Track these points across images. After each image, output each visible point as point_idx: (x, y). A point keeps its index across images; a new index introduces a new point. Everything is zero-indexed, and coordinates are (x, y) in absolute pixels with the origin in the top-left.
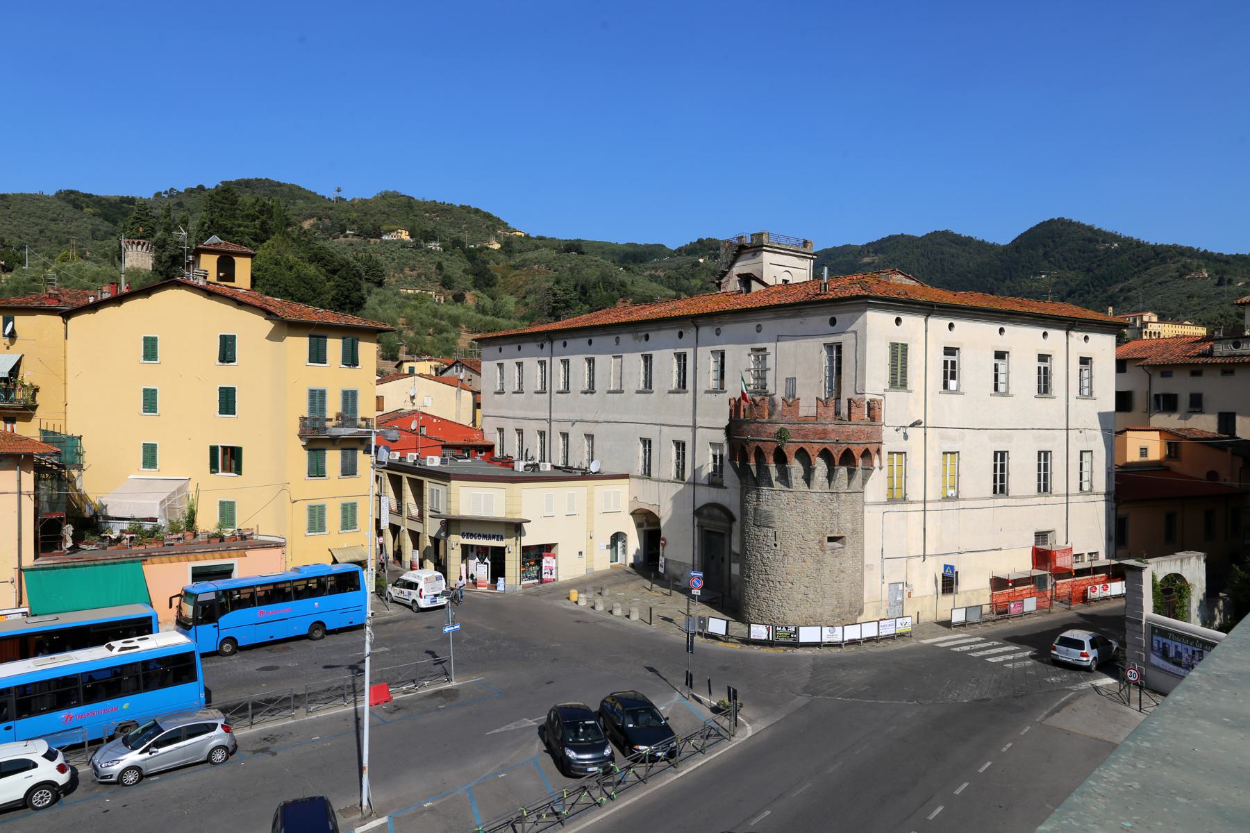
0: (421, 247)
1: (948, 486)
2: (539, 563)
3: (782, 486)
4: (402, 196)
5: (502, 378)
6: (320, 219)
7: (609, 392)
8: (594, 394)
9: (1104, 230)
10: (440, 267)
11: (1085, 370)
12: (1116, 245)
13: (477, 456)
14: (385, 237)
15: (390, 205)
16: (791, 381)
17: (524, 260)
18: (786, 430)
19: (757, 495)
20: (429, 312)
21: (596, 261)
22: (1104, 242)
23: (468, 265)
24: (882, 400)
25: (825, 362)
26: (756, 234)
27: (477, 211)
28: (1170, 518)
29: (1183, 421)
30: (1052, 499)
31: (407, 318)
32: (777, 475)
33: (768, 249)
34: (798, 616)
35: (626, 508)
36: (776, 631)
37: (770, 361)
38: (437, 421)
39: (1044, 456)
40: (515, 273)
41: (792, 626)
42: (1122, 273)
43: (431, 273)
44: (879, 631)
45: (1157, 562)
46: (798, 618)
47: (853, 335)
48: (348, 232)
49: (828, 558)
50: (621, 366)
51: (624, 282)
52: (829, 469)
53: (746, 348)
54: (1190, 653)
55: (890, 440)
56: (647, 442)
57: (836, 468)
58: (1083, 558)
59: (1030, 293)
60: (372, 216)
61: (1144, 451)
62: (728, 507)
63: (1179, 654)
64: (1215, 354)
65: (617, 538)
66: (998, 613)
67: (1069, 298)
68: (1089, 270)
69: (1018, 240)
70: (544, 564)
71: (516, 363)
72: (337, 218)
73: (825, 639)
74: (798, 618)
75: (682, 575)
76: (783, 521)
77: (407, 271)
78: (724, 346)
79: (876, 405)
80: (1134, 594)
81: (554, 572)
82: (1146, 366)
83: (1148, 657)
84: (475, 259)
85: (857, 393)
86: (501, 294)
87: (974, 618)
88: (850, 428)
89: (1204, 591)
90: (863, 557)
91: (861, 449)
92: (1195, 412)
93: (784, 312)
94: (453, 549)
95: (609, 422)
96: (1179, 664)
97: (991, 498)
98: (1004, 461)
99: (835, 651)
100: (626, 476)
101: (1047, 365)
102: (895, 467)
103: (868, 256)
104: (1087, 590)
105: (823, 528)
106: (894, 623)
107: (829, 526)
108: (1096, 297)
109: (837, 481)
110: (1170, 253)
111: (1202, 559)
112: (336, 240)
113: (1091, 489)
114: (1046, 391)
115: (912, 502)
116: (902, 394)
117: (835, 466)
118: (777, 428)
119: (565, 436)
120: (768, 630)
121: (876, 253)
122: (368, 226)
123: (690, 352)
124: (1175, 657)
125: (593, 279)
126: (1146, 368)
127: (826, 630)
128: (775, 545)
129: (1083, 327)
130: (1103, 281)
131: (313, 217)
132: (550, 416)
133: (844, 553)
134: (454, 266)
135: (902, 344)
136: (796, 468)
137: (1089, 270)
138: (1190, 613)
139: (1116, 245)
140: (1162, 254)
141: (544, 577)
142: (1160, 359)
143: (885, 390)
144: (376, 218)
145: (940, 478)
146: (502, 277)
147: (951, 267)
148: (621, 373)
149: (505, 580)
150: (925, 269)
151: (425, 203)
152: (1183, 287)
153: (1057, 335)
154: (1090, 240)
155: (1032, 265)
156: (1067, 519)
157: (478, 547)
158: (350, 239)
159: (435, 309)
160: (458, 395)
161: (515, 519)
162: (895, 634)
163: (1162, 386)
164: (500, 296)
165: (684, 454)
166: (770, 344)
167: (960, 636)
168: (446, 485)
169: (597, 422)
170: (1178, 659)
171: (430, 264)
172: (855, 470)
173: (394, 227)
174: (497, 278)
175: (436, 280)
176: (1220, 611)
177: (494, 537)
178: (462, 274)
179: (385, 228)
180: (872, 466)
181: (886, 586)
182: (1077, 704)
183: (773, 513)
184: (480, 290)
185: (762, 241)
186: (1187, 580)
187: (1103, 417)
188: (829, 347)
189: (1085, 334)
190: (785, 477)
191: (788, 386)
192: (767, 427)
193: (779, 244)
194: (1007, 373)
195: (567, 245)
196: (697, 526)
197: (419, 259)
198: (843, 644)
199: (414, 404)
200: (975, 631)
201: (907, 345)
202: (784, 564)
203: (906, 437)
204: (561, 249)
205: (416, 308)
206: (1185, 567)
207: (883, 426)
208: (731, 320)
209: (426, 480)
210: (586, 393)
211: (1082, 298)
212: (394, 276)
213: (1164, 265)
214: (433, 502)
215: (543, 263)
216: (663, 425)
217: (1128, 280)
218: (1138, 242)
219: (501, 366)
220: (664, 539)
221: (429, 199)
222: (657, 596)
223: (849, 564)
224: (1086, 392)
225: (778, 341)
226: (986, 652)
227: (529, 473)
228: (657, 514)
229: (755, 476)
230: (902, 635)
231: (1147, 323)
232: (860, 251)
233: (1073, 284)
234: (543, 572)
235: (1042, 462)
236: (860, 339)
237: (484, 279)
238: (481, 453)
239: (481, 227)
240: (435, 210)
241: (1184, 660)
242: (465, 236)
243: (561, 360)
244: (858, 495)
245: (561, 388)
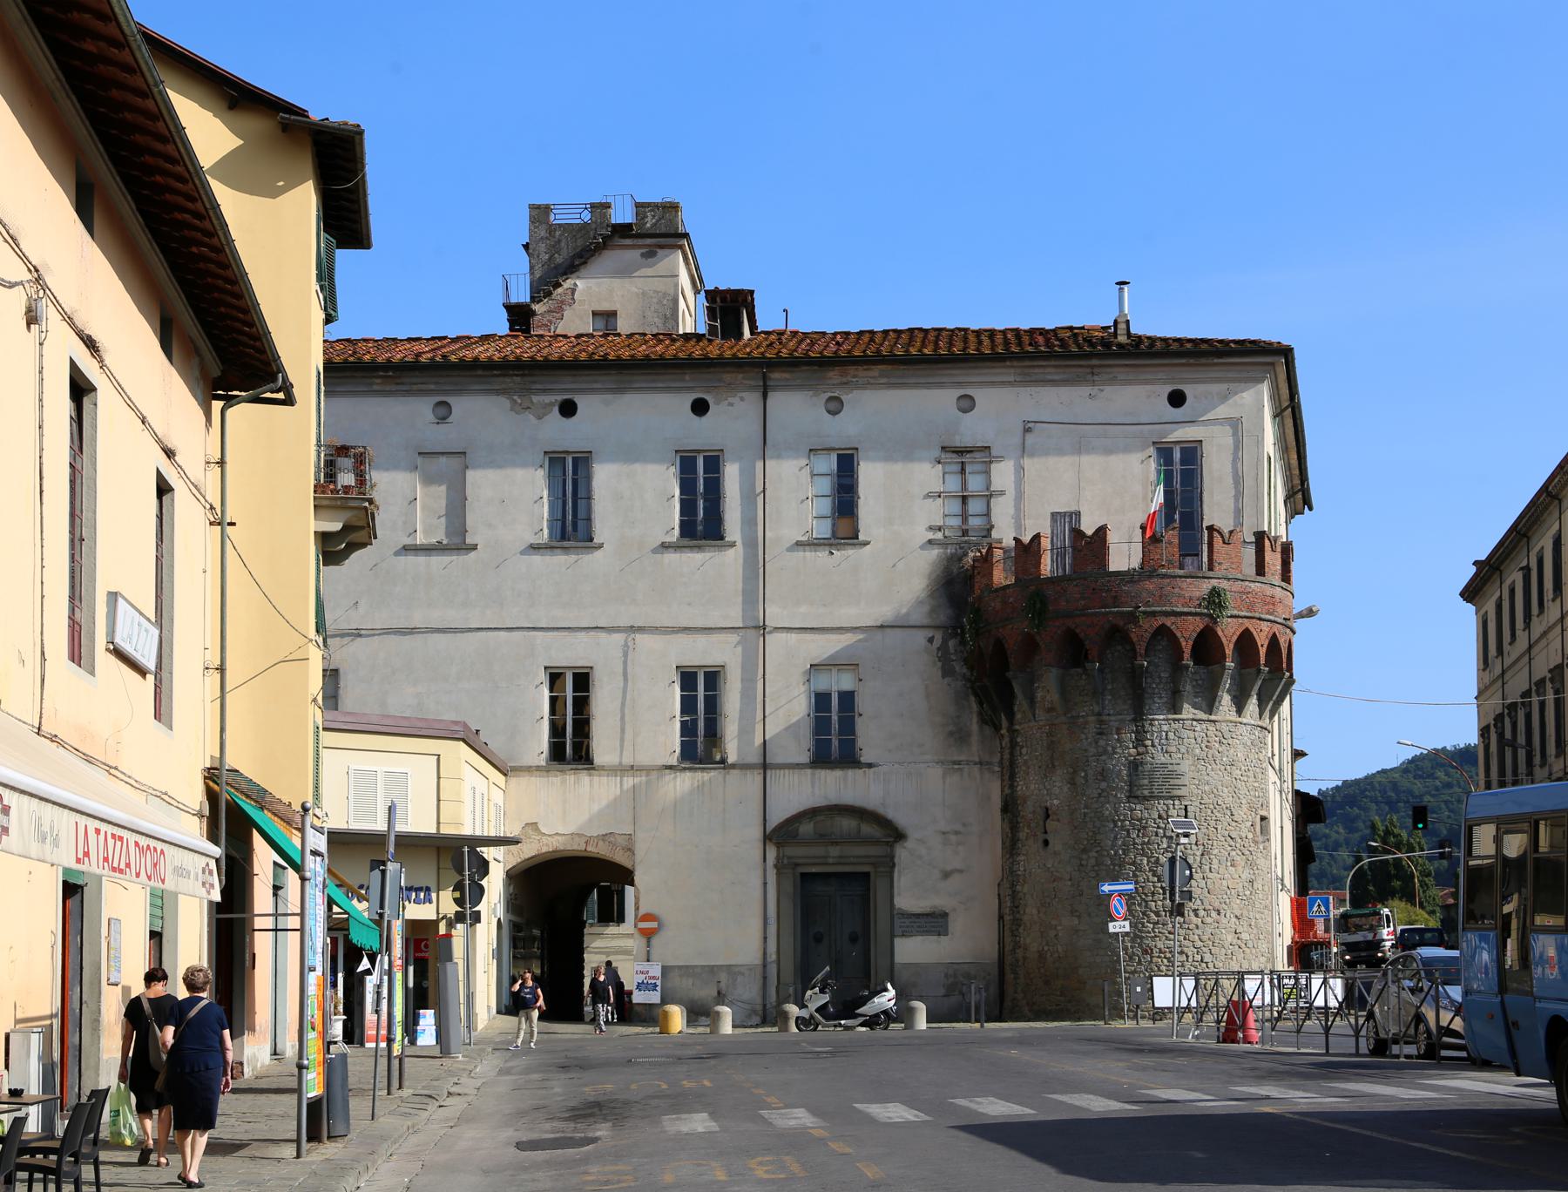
19: (1137, 732)
26: (655, 206)
62: (881, 811)
93: (1053, 370)
118: (1205, 587)
192: (1184, 585)
208: (884, 380)
216: (641, 629)
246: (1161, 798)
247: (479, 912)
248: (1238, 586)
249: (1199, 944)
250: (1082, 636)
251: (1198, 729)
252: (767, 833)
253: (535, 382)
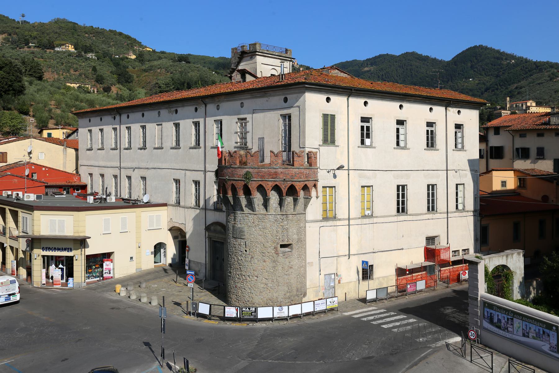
0: (82, 56)
1: (366, 208)
2: (102, 266)
3: (250, 211)
4: (69, 22)
5: (91, 140)
6: (10, 35)
7: (155, 148)
8: (146, 150)
9: (506, 52)
10: (94, 69)
11: (459, 132)
12: (513, 61)
13: (75, 192)
14: (57, 49)
15: (60, 28)
16: (262, 139)
17: (152, 66)
18: (250, 172)
20: (72, 97)
21: (198, 68)
22: (506, 59)
23: (114, 69)
24: (317, 152)
25: (282, 127)
26: (252, 44)
27: (121, 34)
28: (516, 226)
29: (533, 164)
30: (437, 216)
31: (56, 101)
32: (246, 203)
33: (260, 54)
34: (262, 299)
35: (165, 226)
36: (242, 311)
37: (249, 127)
38: (45, 169)
39: (431, 188)
40: (145, 75)
41: (253, 307)
42: (517, 77)
43: (88, 73)
44: (314, 308)
45: (490, 258)
46: (261, 301)
47: (298, 109)
48: (30, 44)
49: (281, 259)
50: (162, 131)
51: (214, 81)
52: (280, 198)
53: (235, 118)
54: (506, 320)
55: (324, 179)
56: (177, 181)
57: (284, 198)
58: (459, 253)
59: (463, 89)
60: (48, 34)
61: (504, 183)
63: (499, 320)
64: (551, 123)
65: (159, 248)
66: (400, 292)
67: (486, 93)
68: (497, 76)
69: (456, 58)
70: (105, 266)
71: (100, 129)
72: (22, 35)
73: (276, 315)
74: (261, 301)
75: (199, 271)
76: (251, 234)
77: (72, 71)
78: (221, 117)
79: (312, 155)
80: (474, 278)
81: (112, 272)
82: (510, 130)
83: (481, 322)
84: (119, 65)
85: (300, 148)
86: (136, 88)
87: (382, 295)
88: (293, 171)
89: (523, 275)
90: (305, 257)
91: (271, 184)
92: (540, 159)
93: (256, 94)
94: (36, 259)
95: (155, 168)
96: (499, 327)
97: (395, 216)
98: (404, 191)
99: (282, 323)
100: (165, 205)
101: (433, 129)
102: (328, 196)
103: (367, 67)
104: (460, 274)
105: (277, 239)
106: (325, 302)
107: (281, 237)
108: (501, 92)
109: (286, 207)
110: (544, 66)
111: (521, 255)
112: (21, 50)
113: (464, 209)
114: (432, 146)
115: (340, 220)
116: (331, 148)
117: (283, 196)
118: (244, 171)
119: (129, 178)
120: (237, 310)
121: (372, 64)
122: (45, 41)
123: (201, 121)
124: (497, 323)
125: (195, 79)
126: (511, 132)
127: (276, 309)
128: (246, 251)
129: (456, 104)
130: (506, 83)
131: (4, 33)
132: (120, 165)
133: (292, 255)
134: (104, 69)
135: (331, 115)
136: (258, 198)
137: (497, 76)
138: (513, 291)
139: (513, 61)
140: (539, 67)
141: (104, 275)
142: (519, 127)
143: (319, 146)
144: (51, 36)
145: (359, 204)
146: (137, 77)
147: (416, 74)
148: (162, 136)
149: (73, 279)
150: (401, 75)
151: (85, 27)
152: (552, 86)
153: (439, 110)
154: (498, 58)
155: (464, 73)
156: (448, 228)
157: (56, 257)
158: (32, 49)
159: (77, 95)
160: (64, 151)
161: (80, 237)
162: (326, 309)
163: (520, 143)
164: (136, 89)
165: (199, 189)
166: (249, 115)
167: (371, 309)
168: (31, 214)
169: (148, 168)
170: (499, 324)
171: (88, 67)
172: (297, 199)
173: (64, 42)
174: (133, 77)
175: (92, 78)
176: (534, 289)
177: (65, 249)
178: (110, 74)
179: (57, 42)
180: (310, 196)
181: (322, 276)
182: (431, 358)
183: (244, 229)
184: (122, 84)
185: (256, 48)
186: (511, 269)
187: (471, 162)
188: (284, 116)
189: (458, 109)
190: (250, 205)
191: (260, 144)
193: (268, 51)
194: (405, 134)
195: (179, 57)
196: (208, 237)
197: (80, 64)
198: (288, 318)
199: (31, 158)
200: (382, 305)
201: (334, 115)
202: (251, 264)
203: (335, 176)
204: (176, 60)
205: (63, 94)
206: (509, 260)
207: (319, 169)
208: (225, 100)
209: (20, 211)
210: (141, 149)
211: (493, 92)
212: (62, 75)
213: (541, 73)
214: (23, 226)
215: (164, 68)
216: (187, 170)
217: (520, 82)
218: (526, 59)
219: (90, 131)
220: (188, 247)
221: (88, 25)
222: (178, 287)
223: (295, 262)
224: (459, 146)
225: (253, 113)
226: (383, 321)
227: (97, 204)
228: (184, 230)
229: (232, 204)
230: (332, 310)
231: (529, 107)
232: (362, 64)
233: (488, 84)
234: (104, 272)
235: (431, 192)
236: (302, 111)
237: (125, 77)
238: (78, 190)
239: (123, 44)
240: (92, 32)
241: (502, 324)
242: (113, 50)
243: (126, 127)
244: (302, 215)
245: (127, 146)
246: (239, 238)
248: (256, 170)
249: (250, 287)
251: (250, 217)
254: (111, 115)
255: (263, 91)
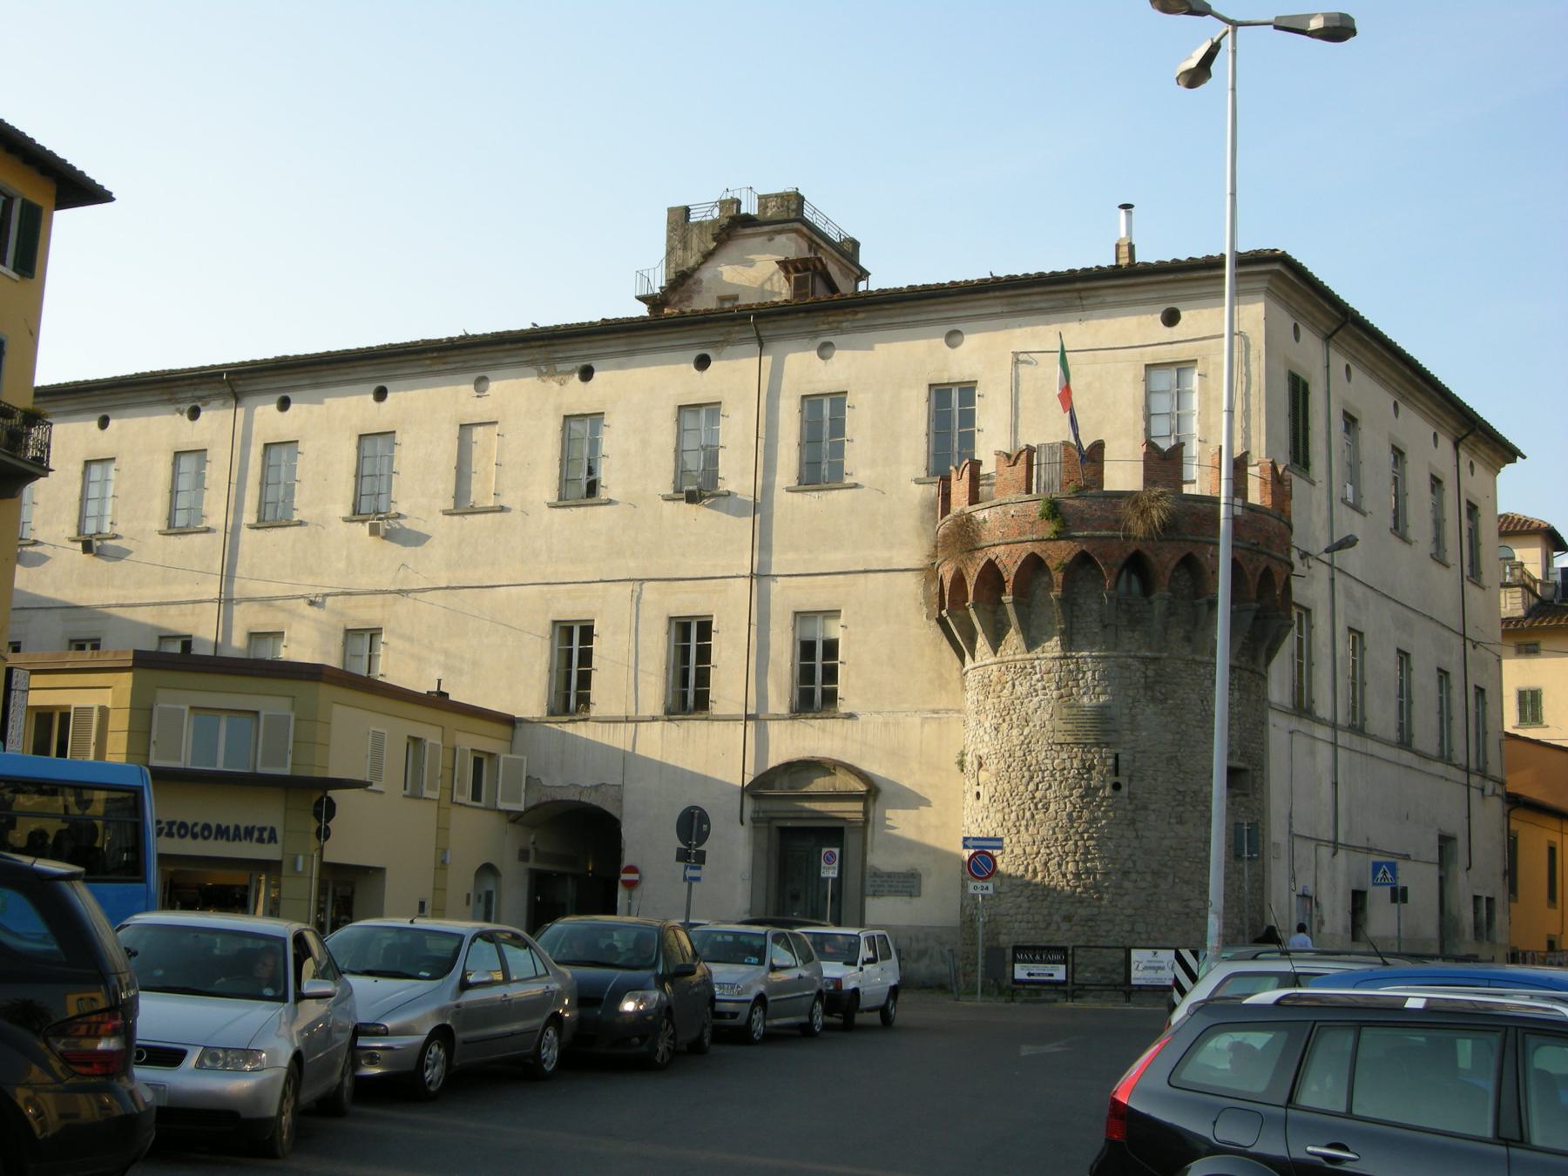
62: (602, 806)
247: (705, 852)
250: (1000, 566)
252: (745, 785)
253: (557, 352)
254: (172, 401)
255: (1079, 285)
